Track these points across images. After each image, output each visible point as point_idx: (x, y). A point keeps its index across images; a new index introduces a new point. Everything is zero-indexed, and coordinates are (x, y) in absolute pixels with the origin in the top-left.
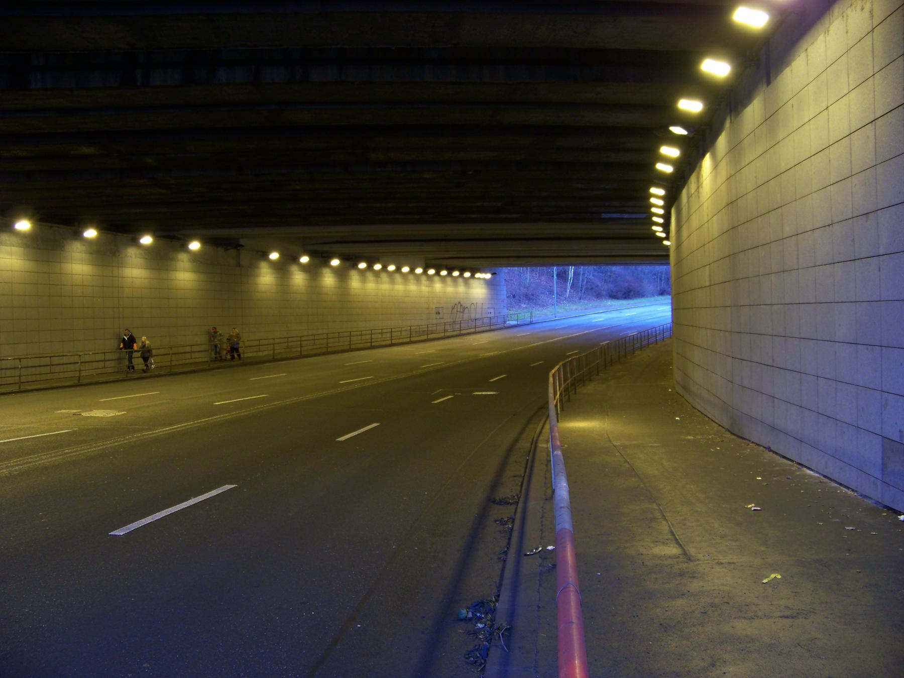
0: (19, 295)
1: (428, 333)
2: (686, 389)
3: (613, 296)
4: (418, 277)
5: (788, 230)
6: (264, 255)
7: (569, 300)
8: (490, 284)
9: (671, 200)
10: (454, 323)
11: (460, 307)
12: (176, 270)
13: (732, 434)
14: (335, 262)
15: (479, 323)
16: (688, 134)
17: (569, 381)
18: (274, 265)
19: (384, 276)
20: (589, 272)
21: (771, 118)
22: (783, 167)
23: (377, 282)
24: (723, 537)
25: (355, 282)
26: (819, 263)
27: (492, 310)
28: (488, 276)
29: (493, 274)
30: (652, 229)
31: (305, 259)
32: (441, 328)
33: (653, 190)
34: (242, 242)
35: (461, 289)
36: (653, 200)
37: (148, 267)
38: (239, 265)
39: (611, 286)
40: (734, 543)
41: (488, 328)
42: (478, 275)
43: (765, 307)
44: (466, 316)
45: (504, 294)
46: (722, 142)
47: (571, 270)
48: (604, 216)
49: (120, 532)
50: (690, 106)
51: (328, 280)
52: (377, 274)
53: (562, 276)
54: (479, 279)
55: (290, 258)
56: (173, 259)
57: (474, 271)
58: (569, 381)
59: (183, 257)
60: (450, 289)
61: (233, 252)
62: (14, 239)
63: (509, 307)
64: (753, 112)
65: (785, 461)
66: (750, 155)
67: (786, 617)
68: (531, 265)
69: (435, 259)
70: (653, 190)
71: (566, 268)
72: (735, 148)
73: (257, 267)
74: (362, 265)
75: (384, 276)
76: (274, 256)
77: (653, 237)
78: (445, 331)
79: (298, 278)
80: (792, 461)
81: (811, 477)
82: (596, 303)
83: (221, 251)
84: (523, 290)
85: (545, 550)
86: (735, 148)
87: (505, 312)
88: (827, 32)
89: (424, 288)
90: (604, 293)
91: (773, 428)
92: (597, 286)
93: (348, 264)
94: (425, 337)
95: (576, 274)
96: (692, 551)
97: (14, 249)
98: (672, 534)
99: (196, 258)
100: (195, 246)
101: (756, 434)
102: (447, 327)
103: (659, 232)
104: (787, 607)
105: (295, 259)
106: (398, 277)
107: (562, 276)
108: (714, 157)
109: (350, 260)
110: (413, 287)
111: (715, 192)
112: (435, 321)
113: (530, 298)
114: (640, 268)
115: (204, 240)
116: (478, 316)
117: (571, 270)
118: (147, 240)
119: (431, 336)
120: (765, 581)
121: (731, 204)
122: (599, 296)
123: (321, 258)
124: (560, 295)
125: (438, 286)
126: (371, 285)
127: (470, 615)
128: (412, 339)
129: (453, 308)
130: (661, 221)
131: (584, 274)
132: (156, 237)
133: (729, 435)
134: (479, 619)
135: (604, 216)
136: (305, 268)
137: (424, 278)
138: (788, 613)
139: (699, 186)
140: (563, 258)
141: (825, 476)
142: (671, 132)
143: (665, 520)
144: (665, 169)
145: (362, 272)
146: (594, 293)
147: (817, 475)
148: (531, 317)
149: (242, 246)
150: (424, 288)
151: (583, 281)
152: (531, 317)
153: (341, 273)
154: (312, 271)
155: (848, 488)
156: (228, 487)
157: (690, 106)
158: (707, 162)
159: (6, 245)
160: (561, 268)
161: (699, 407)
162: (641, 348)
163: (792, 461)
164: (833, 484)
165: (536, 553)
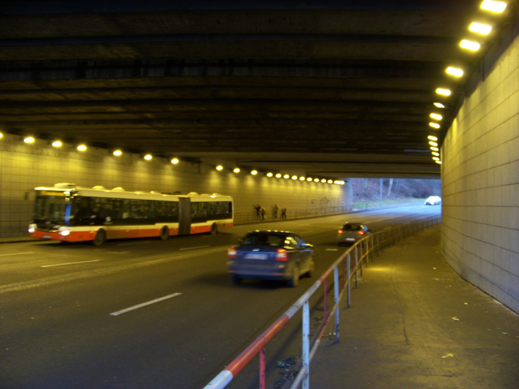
0: (510, 74)
1: (306, 214)
2: (444, 252)
3: (416, 196)
4: (301, 182)
5: (490, 165)
6: (214, 167)
7: (390, 198)
8: (343, 187)
9: (440, 143)
10: (322, 209)
11: (325, 200)
12: (164, 174)
13: (463, 278)
14: (254, 172)
15: (336, 209)
16: (445, 108)
17: (378, 245)
18: (237, 175)
19: (282, 181)
20: (402, 182)
21: (483, 100)
22: (488, 129)
23: (278, 184)
24: (431, 333)
25: (265, 184)
26: (504, 184)
27: (344, 202)
28: (342, 183)
29: (346, 181)
30: (432, 159)
31: (237, 170)
32: (314, 211)
33: (430, 137)
34: (202, 160)
35: (327, 190)
36: (430, 143)
37: (149, 172)
38: (199, 172)
39: (414, 190)
40: (436, 337)
41: (341, 212)
42: (336, 182)
43: (479, 207)
44: (329, 205)
45: (351, 193)
46: (461, 112)
47: (391, 181)
48: (406, 151)
49: (115, 314)
50: (444, 92)
51: (250, 182)
52: (278, 180)
53: (386, 184)
54: (337, 184)
55: (228, 169)
56: (163, 168)
57: (334, 179)
58: (378, 245)
59: (168, 167)
60: (320, 190)
61: (196, 165)
62: (77, 155)
63: (354, 201)
64: (475, 96)
65: (486, 295)
66: (474, 121)
67: (446, 376)
68: (369, 177)
69: (315, 172)
70: (430, 137)
71: (388, 179)
72: (467, 117)
73: (210, 174)
74: (270, 175)
75: (282, 181)
76: (220, 168)
77: (434, 162)
78: (316, 213)
79: (233, 181)
80: (488, 295)
81: (496, 304)
82: (405, 199)
83: (189, 164)
84: (363, 191)
85: (332, 335)
86: (467, 117)
87: (352, 203)
88: (509, 55)
89: (305, 189)
90: (410, 194)
91: (481, 276)
92: (406, 190)
93: (11, 137)
94: (304, 217)
95: (394, 183)
96: (411, 339)
97: (77, 161)
98: (404, 330)
99: (176, 168)
100: (175, 161)
101: (473, 279)
102: (318, 211)
103: (437, 161)
104: (449, 371)
105: (231, 170)
106: (290, 182)
107: (386, 184)
108: (458, 121)
109: (263, 172)
110: (298, 188)
111: (458, 141)
112: (311, 208)
113: (367, 196)
114: (432, 180)
115: (181, 158)
116: (336, 205)
117: (391, 181)
118: (148, 157)
119: (308, 216)
120: (444, 357)
121: (465, 148)
122: (407, 196)
123: (246, 170)
124: (384, 194)
125: (313, 188)
126: (275, 186)
127: (283, 365)
128: (298, 217)
129: (321, 201)
130: (437, 154)
131: (399, 183)
132: (154, 155)
133: (460, 279)
134: (288, 367)
135: (406, 151)
136: (237, 175)
137: (305, 183)
138: (448, 374)
139: (451, 136)
140: (387, 174)
141: (504, 305)
142: (434, 106)
143: (404, 323)
144: (436, 126)
145: (269, 178)
146: (404, 194)
147: (500, 304)
148: (367, 207)
149: (201, 162)
150: (305, 189)
151: (398, 187)
152: (367, 207)
153: (257, 179)
154: (241, 177)
155: (514, 311)
156: (177, 294)
157: (444, 92)
158: (455, 123)
159: (73, 158)
160: (385, 179)
161: (449, 262)
162: (428, 227)
163: (488, 295)
164: (508, 309)
165: (327, 336)
